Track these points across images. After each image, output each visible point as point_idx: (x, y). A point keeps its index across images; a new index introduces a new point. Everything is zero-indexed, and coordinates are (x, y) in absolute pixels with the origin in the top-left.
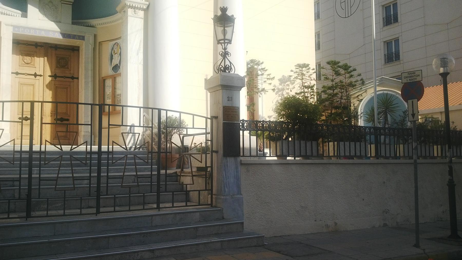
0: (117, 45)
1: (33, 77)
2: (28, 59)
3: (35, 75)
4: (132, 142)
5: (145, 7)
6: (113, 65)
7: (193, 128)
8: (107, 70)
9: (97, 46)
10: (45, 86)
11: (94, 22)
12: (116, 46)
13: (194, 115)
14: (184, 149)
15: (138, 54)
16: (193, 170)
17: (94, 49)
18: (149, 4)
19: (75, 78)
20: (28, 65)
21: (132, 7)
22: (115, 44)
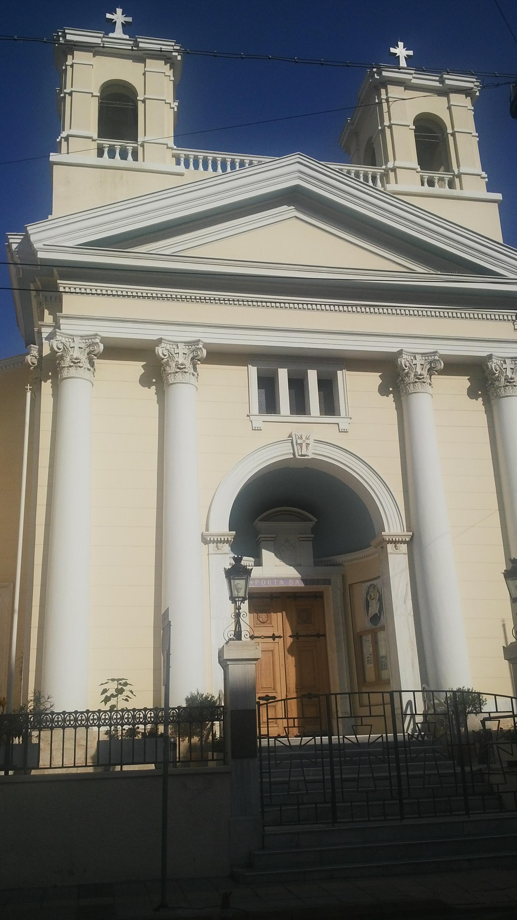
0: (374, 588)
1: (271, 640)
2: (263, 616)
3: (274, 637)
4: (411, 726)
5: (407, 539)
6: (370, 616)
7: (497, 712)
8: (363, 622)
9: (347, 590)
10: (286, 651)
11: (340, 559)
12: (372, 589)
13: (495, 695)
14: (485, 734)
15: (405, 602)
16: (503, 766)
17: (344, 595)
18: (413, 534)
19: (321, 635)
20: (264, 625)
21: (392, 542)
22: (371, 585)
